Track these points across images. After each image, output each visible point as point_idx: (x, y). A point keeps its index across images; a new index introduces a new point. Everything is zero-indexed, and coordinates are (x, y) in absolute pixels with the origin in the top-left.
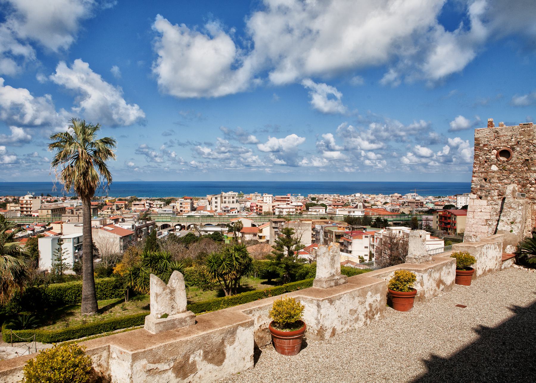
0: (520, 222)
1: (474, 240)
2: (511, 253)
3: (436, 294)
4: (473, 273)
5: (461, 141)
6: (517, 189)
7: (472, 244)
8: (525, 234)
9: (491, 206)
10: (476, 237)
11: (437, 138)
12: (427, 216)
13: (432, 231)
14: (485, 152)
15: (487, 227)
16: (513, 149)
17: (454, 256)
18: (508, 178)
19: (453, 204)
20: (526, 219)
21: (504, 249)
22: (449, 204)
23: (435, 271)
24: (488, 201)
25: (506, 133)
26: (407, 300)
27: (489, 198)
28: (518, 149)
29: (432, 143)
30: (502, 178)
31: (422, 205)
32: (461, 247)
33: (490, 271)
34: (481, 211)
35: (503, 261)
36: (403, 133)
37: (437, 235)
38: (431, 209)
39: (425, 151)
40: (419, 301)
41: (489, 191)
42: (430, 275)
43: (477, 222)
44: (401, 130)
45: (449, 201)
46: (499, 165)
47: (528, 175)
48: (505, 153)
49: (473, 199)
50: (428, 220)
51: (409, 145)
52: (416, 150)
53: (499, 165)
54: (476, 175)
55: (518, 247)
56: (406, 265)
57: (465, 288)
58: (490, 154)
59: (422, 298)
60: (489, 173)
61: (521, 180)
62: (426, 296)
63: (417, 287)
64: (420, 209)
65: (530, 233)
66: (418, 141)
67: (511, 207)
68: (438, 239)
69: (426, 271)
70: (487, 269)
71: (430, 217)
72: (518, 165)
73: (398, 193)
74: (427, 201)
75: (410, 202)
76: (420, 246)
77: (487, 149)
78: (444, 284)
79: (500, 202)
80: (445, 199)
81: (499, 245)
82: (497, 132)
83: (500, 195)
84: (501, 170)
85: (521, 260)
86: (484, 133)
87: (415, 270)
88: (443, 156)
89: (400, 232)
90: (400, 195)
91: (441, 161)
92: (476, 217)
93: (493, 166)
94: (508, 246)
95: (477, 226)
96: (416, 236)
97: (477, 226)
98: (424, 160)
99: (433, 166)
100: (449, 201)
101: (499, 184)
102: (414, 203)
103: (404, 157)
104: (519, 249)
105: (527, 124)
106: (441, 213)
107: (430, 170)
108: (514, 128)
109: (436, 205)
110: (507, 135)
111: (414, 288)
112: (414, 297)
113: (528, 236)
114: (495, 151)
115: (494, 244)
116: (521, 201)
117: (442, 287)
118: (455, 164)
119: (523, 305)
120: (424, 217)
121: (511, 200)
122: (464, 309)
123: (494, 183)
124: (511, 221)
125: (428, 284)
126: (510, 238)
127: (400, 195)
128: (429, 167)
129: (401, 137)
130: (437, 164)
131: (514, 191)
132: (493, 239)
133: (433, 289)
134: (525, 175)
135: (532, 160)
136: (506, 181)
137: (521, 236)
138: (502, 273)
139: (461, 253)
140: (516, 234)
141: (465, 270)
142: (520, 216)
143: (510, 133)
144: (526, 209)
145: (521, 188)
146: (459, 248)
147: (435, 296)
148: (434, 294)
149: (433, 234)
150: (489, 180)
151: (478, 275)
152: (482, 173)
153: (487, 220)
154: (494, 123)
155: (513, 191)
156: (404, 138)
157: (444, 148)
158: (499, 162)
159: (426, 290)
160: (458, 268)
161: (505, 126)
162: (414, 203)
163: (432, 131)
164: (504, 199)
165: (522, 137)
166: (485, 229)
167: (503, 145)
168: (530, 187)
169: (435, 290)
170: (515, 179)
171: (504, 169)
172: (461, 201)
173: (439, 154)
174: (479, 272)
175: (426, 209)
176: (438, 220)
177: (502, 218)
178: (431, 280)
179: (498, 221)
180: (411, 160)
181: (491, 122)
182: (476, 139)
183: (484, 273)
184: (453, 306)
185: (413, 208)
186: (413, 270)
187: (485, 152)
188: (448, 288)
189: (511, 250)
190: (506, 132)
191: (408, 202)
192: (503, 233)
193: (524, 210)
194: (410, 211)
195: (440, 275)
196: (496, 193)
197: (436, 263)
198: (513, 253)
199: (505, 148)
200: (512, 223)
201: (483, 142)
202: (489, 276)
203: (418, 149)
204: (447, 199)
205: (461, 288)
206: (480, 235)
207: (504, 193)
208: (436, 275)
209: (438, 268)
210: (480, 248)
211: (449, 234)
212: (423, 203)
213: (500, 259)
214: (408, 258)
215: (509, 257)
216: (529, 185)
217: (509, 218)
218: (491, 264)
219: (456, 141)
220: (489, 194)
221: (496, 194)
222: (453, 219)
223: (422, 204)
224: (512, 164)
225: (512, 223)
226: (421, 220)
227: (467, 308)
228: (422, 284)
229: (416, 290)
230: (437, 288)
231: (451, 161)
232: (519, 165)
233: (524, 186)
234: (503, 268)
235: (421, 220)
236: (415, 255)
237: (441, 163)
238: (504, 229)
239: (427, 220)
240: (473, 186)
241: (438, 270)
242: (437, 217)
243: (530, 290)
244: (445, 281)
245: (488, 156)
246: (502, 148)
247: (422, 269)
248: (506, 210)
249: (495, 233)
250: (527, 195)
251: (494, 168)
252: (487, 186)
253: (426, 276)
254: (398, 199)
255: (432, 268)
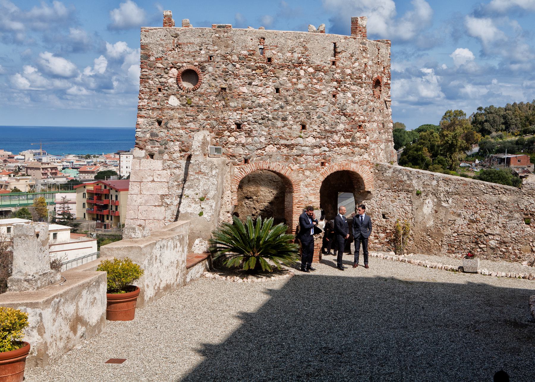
0: (213, 198)
1: (139, 234)
2: (201, 252)
3: (70, 345)
4: (137, 295)
5: (128, 49)
6: (209, 139)
7: (136, 242)
8: (222, 218)
9: (169, 171)
10: (144, 228)
11: (85, 41)
12: (64, 195)
13: (75, 222)
14: (159, 71)
15: (163, 208)
16: (203, 69)
17: (105, 267)
18: (195, 120)
19: (114, 169)
20: (223, 192)
21: (190, 246)
22: (105, 169)
23: (66, 300)
24: (164, 161)
25: (192, 40)
26: (9, 367)
27: (166, 156)
28: (210, 69)
29: (74, 49)
30: (185, 120)
31: (55, 174)
32: (118, 249)
33: (168, 288)
34: (153, 181)
35: (188, 268)
36: (17, 26)
37: (84, 230)
38: (72, 180)
39: (61, 65)
40: (37, 365)
41: (166, 144)
42: (57, 311)
43: (147, 201)
44: (14, 18)
45: (105, 164)
46: (182, 96)
47: (225, 115)
48: (190, 75)
49: (139, 158)
50: (67, 203)
51: (28, 51)
52: (43, 62)
53: (182, 96)
54: (143, 113)
55: (211, 241)
56: (7, 296)
57: (125, 326)
58: (166, 76)
59: (41, 359)
60: (166, 111)
61: (215, 123)
62: (50, 352)
63: (31, 338)
64: (52, 181)
65: (229, 215)
66: (49, 43)
67: (200, 172)
68: (85, 238)
69: (47, 302)
70: (162, 285)
71: (71, 196)
72: (211, 98)
73: (6, 150)
74: (65, 163)
75: (31, 168)
76: (36, 253)
77: (161, 66)
78: (84, 323)
79: (183, 162)
80: (99, 160)
81: (181, 240)
82: (176, 36)
83: (184, 151)
84: (184, 105)
85: (216, 264)
86: (157, 37)
87: (27, 305)
88: (96, 76)
89: (9, 230)
90: (10, 153)
91: (93, 85)
92: (144, 192)
93: (172, 97)
94: (197, 241)
95: (146, 208)
96: (27, 236)
97: (146, 208)
98: (58, 83)
99: (76, 96)
100: (105, 164)
101: (181, 131)
102: (39, 169)
103: (19, 75)
104: (213, 243)
105: (223, 27)
106: (91, 188)
107: (71, 103)
108: (205, 31)
109: (81, 172)
110: (193, 43)
111: (23, 340)
112: (24, 360)
113: (226, 221)
114: (174, 71)
115: (172, 239)
116: (215, 160)
117: (81, 329)
118: (118, 93)
119: (216, 341)
120: (59, 196)
121: (201, 159)
122: (121, 365)
123: (174, 128)
124: (201, 195)
125: (54, 328)
126: (200, 227)
127: (10, 153)
128: (68, 97)
129: (14, 32)
130: (84, 91)
131: (204, 143)
132: (172, 230)
133: (64, 336)
134: (221, 116)
135: (230, 90)
136: (192, 125)
137: (216, 221)
138: (186, 290)
139: (116, 260)
140: (208, 218)
141: (122, 292)
142: (214, 187)
143: (198, 40)
144: (223, 175)
145: (215, 138)
146: (115, 251)
147: (67, 349)
148: (65, 347)
149: (75, 228)
150: (166, 124)
151: (146, 299)
152: (153, 109)
153: (163, 196)
154: (173, 20)
155: (203, 143)
156: (20, 36)
157: (97, 61)
158: (181, 91)
159: (49, 340)
160: (110, 291)
161: (191, 27)
162: (39, 169)
163: (78, 25)
164: (190, 157)
165: (216, 48)
166: (161, 213)
167: (187, 60)
168: (229, 137)
169: (68, 338)
170: (206, 123)
171: (189, 104)
172: (127, 164)
173: (88, 72)
174: (149, 293)
175: (63, 181)
176: (85, 201)
177: (186, 192)
178: (59, 319)
179: (181, 197)
180: (32, 82)
181: (169, 18)
182: (143, 47)
183: (158, 294)
184: (102, 363)
185: (36, 180)
186: (20, 305)
187: (159, 71)
188: (94, 330)
189: (201, 247)
190: (191, 38)
191: (27, 168)
192: (188, 218)
193: (220, 177)
194: (31, 186)
195: (77, 306)
196: (176, 147)
197: (68, 285)
198: (204, 252)
199: (190, 67)
200: (202, 199)
201: (155, 53)
202: (166, 297)
203: (47, 61)
204: (101, 159)
205: (118, 326)
206: (152, 225)
207: (189, 148)
208: (69, 309)
209: (73, 293)
210: (149, 249)
211: (106, 226)
212: (56, 168)
213: (183, 266)
214: (12, 280)
215: (200, 259)
216: (227, 133)
217: (197, 192)
218: (169, 276)
219: (119, 48)
220: (166, 148)
221: (177, 149)
222: (114, 198)
223: (55, 172)
224: (201, 95)
225: (202, 199)
226: (53, 203)
227: (126, 362)
228: (41, 330)
229: (27, 344)
230: (71, 334)
231: (109, 87)
232: (213, 97)
233: (219, 134)
234: (188, 280)
235: (53, 203)
236: (27, 274)
237: (93, 90)
238: (190, 210)
239: (65, 202)
240: (139, 134)
241: (73, 298)
242: (84, 196)
243: (226, 314)
244: (86, 317)
245: (163, 80)
246: (186, 66)
247: (41, 301)
248: (192, 178)
249: (176, 219)
250: (223, 150)
251: (174, 101)
252: (163, 133)
253: (48, 313)
254: (5, 161)
255: (61, 295)
